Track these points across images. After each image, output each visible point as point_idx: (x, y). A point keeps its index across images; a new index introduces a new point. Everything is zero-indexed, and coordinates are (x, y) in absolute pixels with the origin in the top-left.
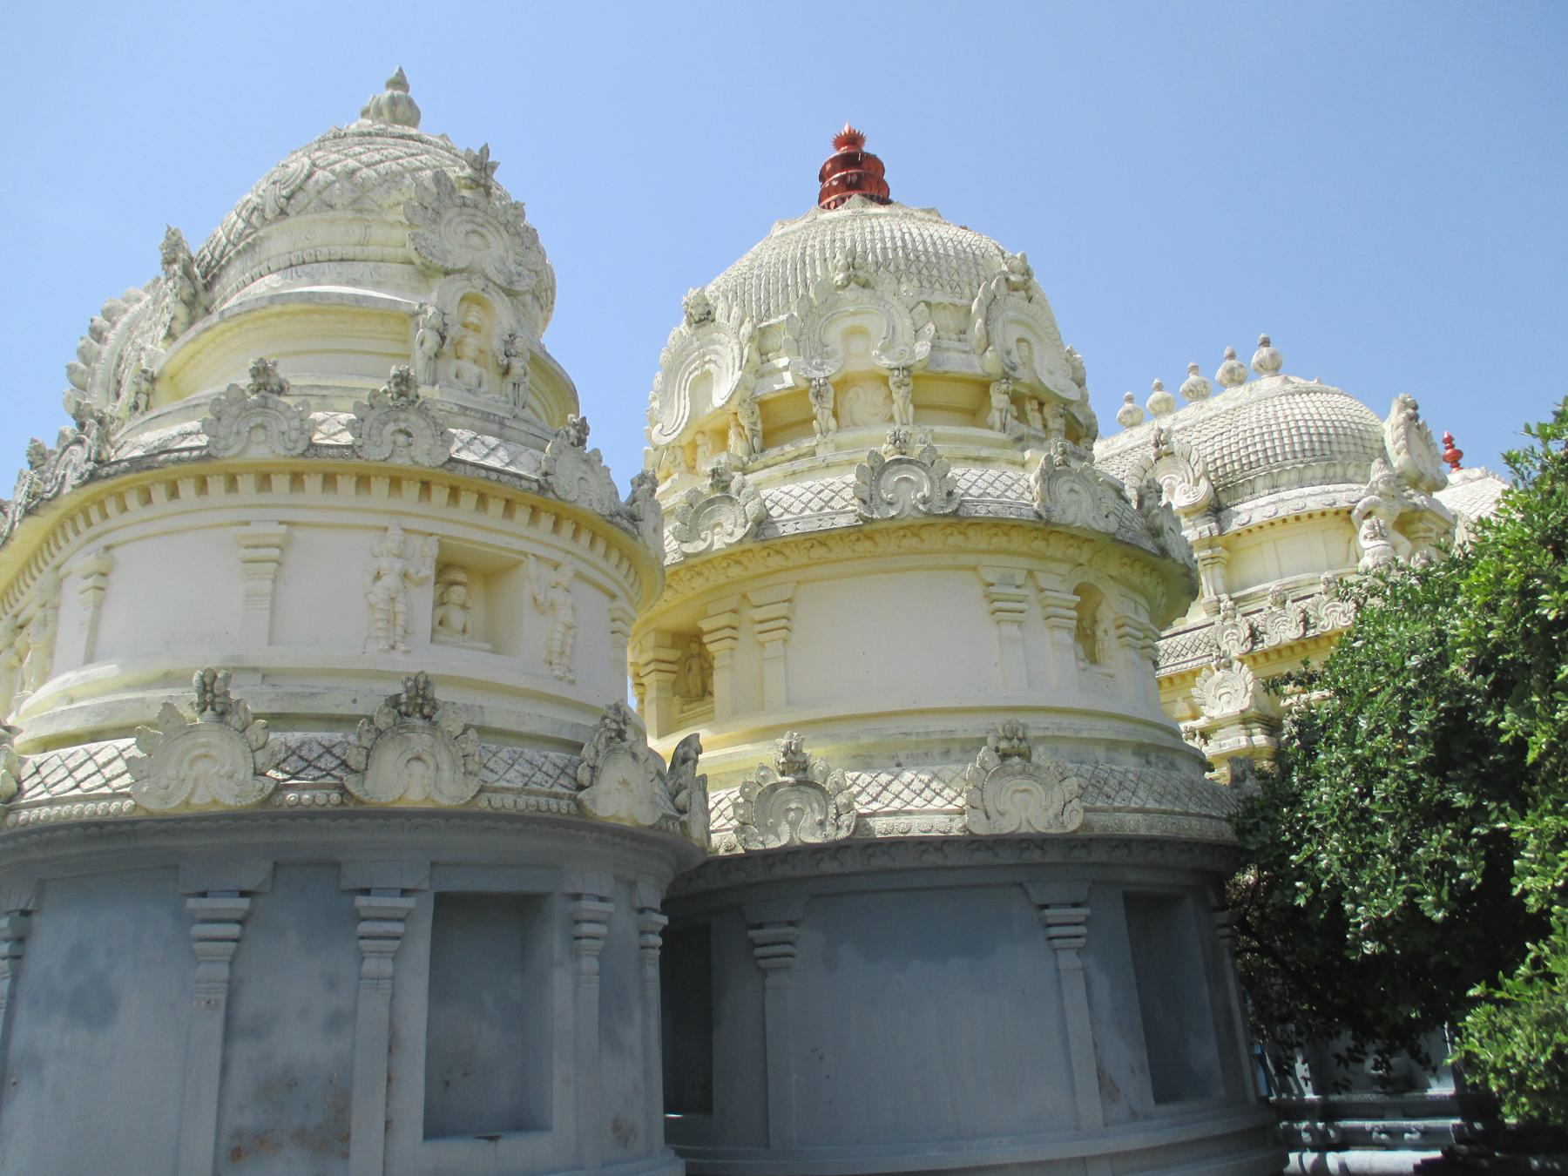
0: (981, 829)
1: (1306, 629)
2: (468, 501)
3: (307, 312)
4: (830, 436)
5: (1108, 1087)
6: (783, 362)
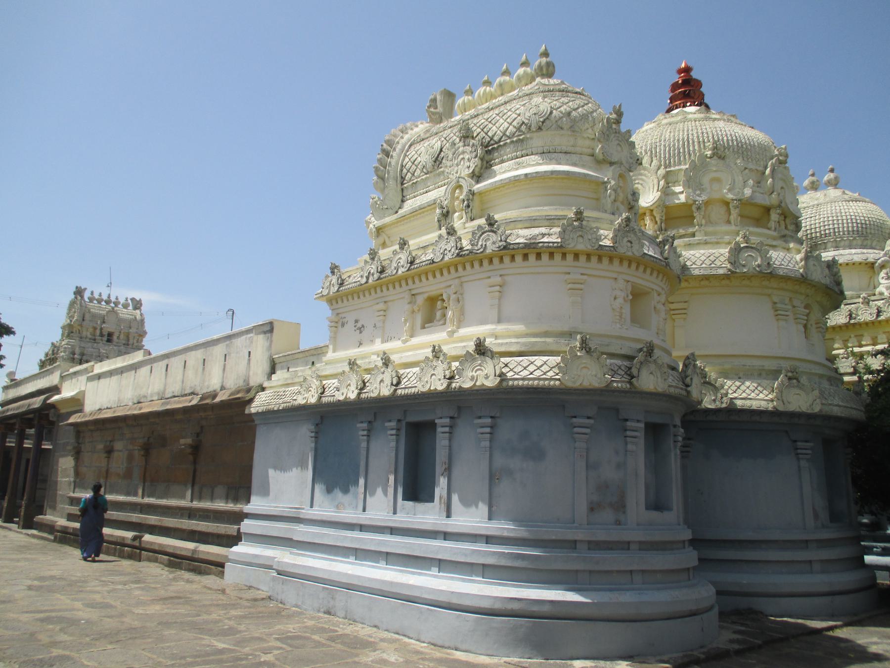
0: (781, 408)
1: (850, 319)
2: (605, 261)
3: (563, 178)
4: (703, 228)
5: (816, 516)
6: (678, 189)
